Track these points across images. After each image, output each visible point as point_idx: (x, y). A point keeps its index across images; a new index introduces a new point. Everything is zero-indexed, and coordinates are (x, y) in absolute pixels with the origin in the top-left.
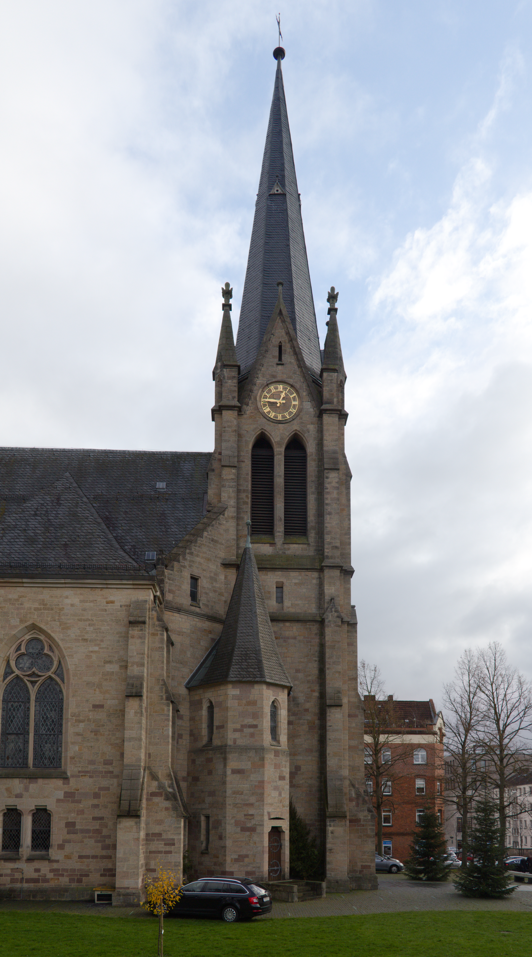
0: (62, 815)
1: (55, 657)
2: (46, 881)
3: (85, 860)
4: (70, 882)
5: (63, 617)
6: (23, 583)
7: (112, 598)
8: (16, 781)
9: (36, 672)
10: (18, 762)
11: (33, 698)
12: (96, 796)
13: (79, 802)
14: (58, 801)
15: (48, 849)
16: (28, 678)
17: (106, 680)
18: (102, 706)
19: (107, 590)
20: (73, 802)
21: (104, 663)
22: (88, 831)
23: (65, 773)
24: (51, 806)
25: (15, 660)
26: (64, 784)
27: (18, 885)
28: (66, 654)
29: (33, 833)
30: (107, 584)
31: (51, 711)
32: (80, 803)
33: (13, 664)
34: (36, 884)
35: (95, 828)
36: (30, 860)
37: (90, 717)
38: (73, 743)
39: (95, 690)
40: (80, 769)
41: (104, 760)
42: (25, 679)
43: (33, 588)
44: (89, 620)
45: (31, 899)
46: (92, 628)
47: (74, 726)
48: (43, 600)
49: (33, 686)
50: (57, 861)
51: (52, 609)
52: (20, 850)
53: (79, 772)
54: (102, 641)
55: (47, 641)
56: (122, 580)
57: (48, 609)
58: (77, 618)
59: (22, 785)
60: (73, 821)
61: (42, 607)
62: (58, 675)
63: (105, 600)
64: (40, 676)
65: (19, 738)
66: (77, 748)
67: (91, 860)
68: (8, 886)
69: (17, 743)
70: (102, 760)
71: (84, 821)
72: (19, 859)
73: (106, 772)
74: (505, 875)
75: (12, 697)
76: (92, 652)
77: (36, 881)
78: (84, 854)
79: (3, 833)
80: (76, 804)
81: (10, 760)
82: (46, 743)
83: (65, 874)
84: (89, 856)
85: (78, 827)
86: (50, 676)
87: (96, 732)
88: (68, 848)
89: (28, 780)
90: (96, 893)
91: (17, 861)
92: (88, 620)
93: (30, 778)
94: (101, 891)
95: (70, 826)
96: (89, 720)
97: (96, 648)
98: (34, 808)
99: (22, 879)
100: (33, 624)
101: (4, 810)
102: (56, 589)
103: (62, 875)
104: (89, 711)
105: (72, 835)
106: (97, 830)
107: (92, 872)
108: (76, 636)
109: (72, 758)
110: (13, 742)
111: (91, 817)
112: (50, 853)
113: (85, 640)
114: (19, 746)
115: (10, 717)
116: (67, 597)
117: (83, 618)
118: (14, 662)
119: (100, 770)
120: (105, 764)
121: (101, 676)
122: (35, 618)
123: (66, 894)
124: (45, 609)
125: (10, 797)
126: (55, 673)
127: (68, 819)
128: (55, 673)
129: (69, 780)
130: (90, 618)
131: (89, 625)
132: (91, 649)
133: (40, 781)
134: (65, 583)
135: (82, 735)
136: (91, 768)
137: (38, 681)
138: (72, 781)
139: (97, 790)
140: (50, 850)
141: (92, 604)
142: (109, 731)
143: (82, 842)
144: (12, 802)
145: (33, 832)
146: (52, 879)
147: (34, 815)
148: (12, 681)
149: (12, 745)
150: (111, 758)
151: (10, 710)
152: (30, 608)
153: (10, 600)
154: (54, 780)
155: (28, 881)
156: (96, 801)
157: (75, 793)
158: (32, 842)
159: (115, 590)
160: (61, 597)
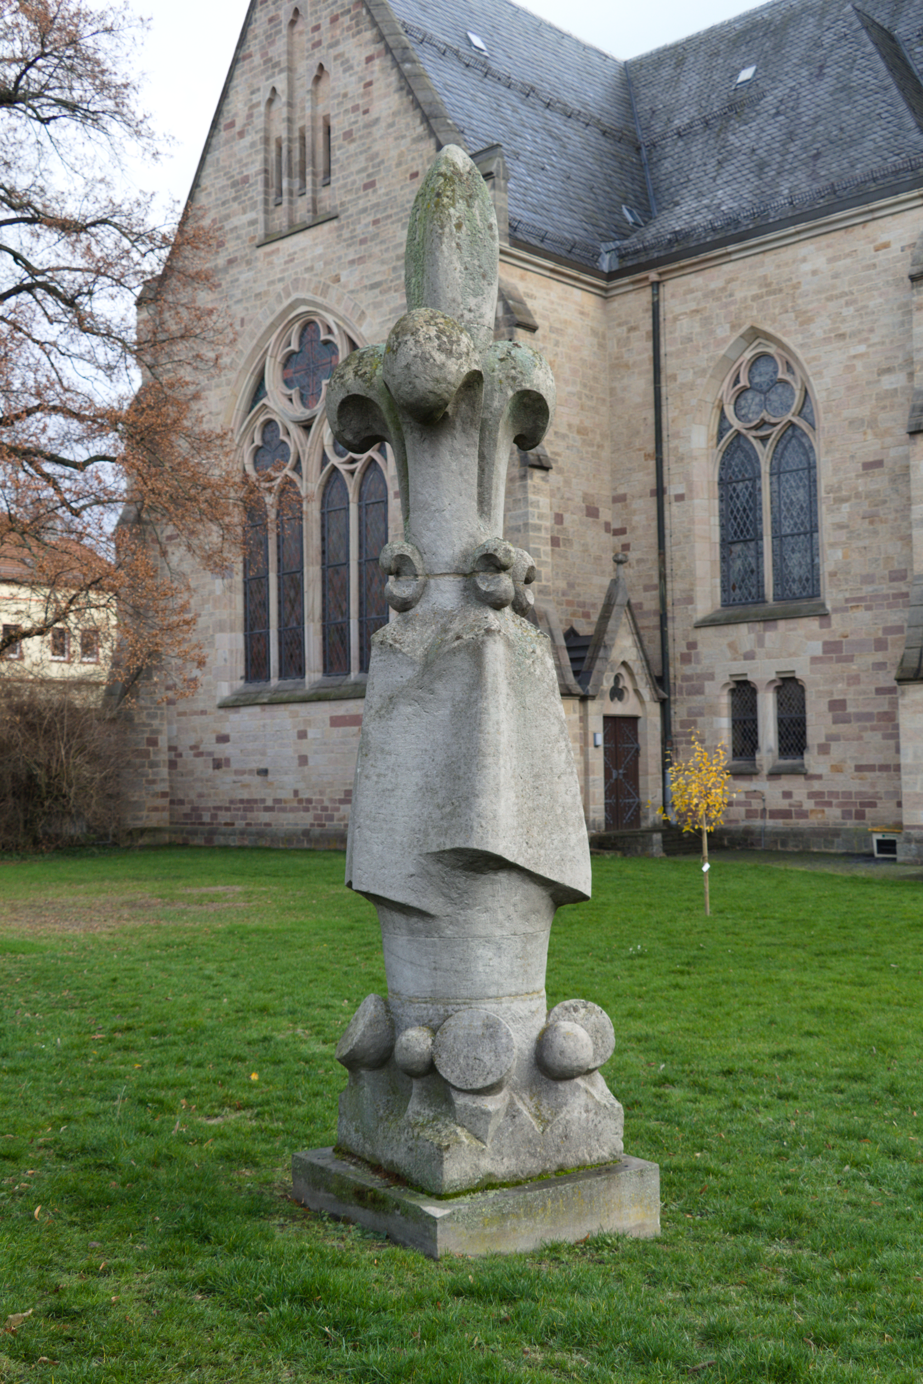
0: (821, 688)
1: (796, 382)
2: (803, 814)
3: (867, 774)
4: (843, 818)
5: (800, 301)
6: (729, 254)
7: (884, 238)
8: (744, 628)
9: (766, 419)
10: (750, 593)
11: (765, 468)
12: (880, 645)
13: (850, 659)
14: (814, 660)
15: (802, 754)
16: (754, 433)
17: (884, 408)
18: (879, 464)
19: (875, 222)
20: (839, 660)
21: (879, 375)
22: (868, 717)
23: (823, 605)
24: (803, 673)
25: (733, 402)
26: (822, 626)
27: (757, 823)
28: (809, 373)
29: (779, 725)
30: (872, 211)
31: (798, 488)
32: (852, 661)
33: (729, 410)
34: (787, 821)
35: (881, 710)
36: (775, 774)
37: (860, 489)
38: (832, 545)
39: (865, 433)
40: (848, 595)
41: (890, 572)
42: (750, 435)
43: (747, 260)
44: (845, 294)
45: (779, 848)
46: (852, 309)
47: (833, 511)
48: (765, 277)
49: (765, 446)
50: (819, 777)
51: (781, 290)
52: (758, 756)
53: (847, 600)
54: (872, 330)
55: (780, 356)
56: (897, 193)
57: (774, 292)
58: (823, 296)
59: (753, 636)
60: (841, 697)
61: (764, 290)
62: (806, 419)
63: (872, 246)
64: (775, 425)
65: (749, 548)
66: (839, 554)
67: (878, 773)
68: (743, 824)
69: (746, 557)
70: (886, 572)
71: (861, 697)
72: (756, 774)
73: (896, 596)
74: (111, 558)
75: (734, 473)
76: (855, 357)
77: (785, 814)
78: (864, 762)
79: (733, 727)
80: (844, 664)
81: (737, 591)
82: (793, 551)
83: (835, 801)
84: (874, 766)
85: (850, 709)
86: (790, 421)
87: (871, 518)
88: (837, 751)
89: (762, 624)
90: (876, 837)
91: (754, 777)
92: (844, 294)
93: (764, 621)
94: (883, 833)
95: (837, 706)
96: (858, 495)
97: (862, 348)
98: (773, 676)
99: (764, 810)
100: (752, 328)
101: (727, 684)
102: (784, 249)
103: (829, 804)
104: (858, 476)
105: (841, 725)
106: (886, 713)
107: (881, 798)
108: (825, 332)
109: (833, 574)
110: (739, 557)
111: (873, 688)
112: (806, 762)
113: (842, 336)
114: (750, 564)
115: (732, 512)
116: (804, 260)
117: (834, 293)
118: (732, 407)
119: (885, 592)
120: (892, 579)
121: (874, 402)
122: (754, 317)
123: (836, 840)
124: (769, 293)
125: (735, 659)
126: (800, 413)
127: (832, 694)
128: (800, 413)
129: (830, 619)
130: (846, 289)
131: (847, 304)
132: (853, 352)
133: (781, 624)
134: (798, 233)
135: (847, 527)
136: (867, 590)
137: (770, 435)
138: (835, 618)
139: (880, 634)
140: (806, 756)
141: (848, 261)
142: (896, 511)
143: (860, 738)
144: (740, 667)
145: (780, 722)
146: (812, 811)
147: (778, 689)
148: (731, 443)
149: (739, 563)
150: (903, 567)
151: (731, 498)
152: (745, 299)
153: (713, 291)
154: (805, 621)
155: (775, 814)
156: (879, 657)
157: (841, 642)
158: (780, 742)
159: (890, 218)
160: (794, 262)
